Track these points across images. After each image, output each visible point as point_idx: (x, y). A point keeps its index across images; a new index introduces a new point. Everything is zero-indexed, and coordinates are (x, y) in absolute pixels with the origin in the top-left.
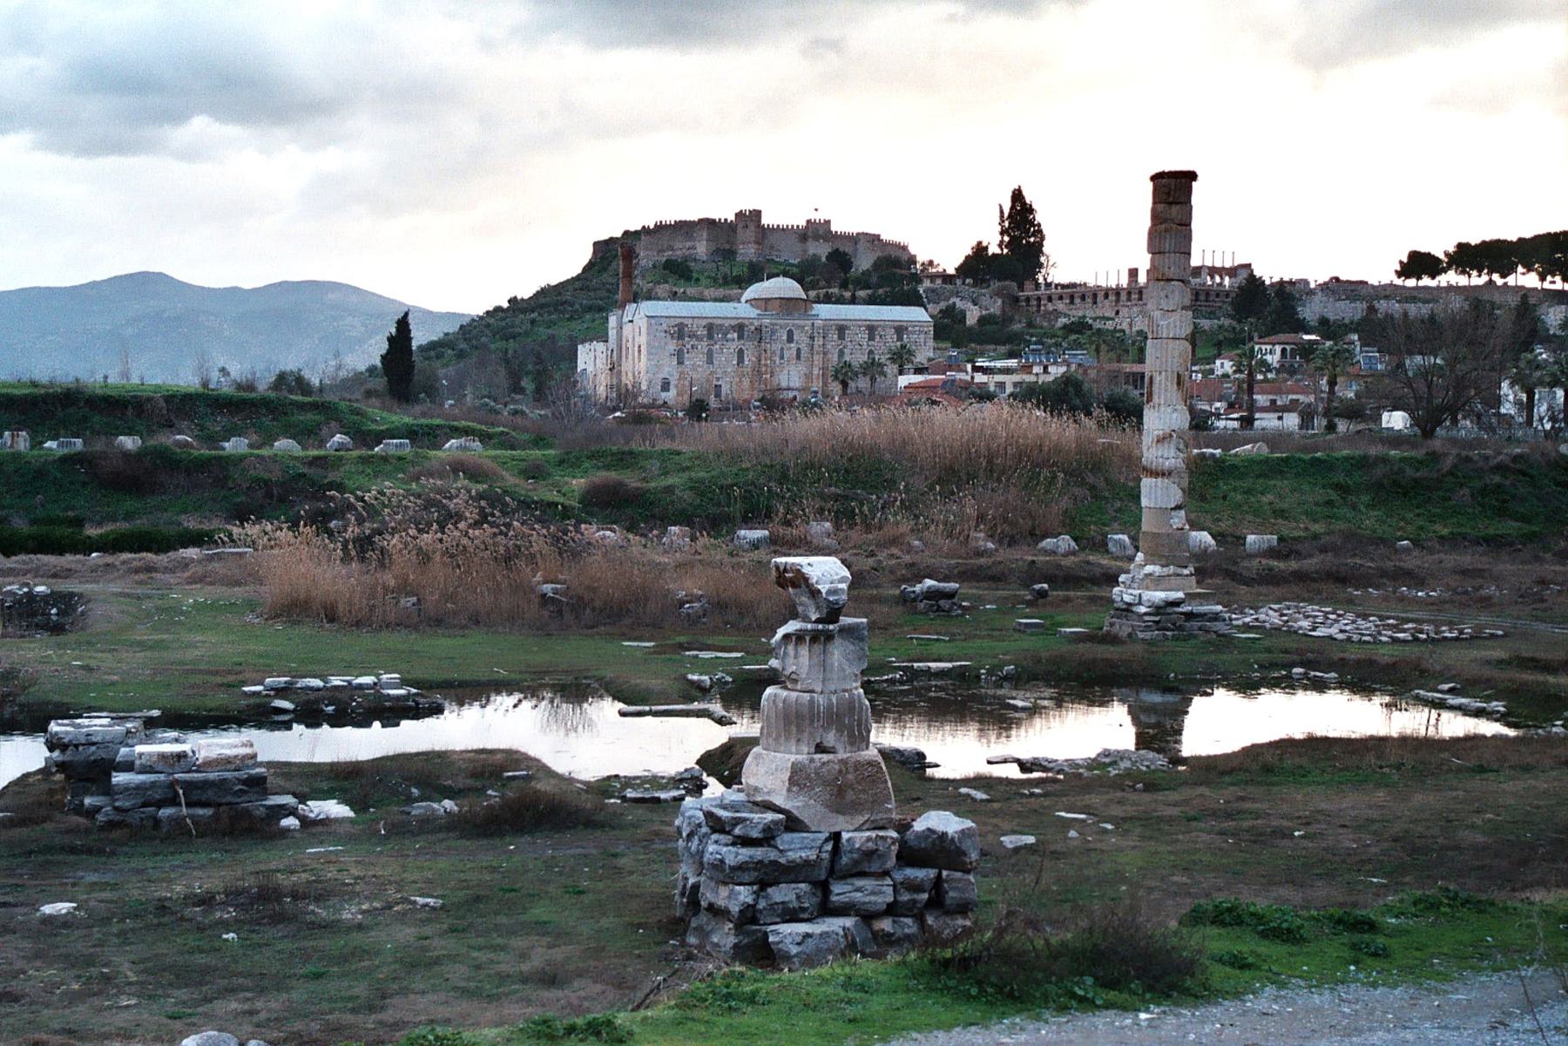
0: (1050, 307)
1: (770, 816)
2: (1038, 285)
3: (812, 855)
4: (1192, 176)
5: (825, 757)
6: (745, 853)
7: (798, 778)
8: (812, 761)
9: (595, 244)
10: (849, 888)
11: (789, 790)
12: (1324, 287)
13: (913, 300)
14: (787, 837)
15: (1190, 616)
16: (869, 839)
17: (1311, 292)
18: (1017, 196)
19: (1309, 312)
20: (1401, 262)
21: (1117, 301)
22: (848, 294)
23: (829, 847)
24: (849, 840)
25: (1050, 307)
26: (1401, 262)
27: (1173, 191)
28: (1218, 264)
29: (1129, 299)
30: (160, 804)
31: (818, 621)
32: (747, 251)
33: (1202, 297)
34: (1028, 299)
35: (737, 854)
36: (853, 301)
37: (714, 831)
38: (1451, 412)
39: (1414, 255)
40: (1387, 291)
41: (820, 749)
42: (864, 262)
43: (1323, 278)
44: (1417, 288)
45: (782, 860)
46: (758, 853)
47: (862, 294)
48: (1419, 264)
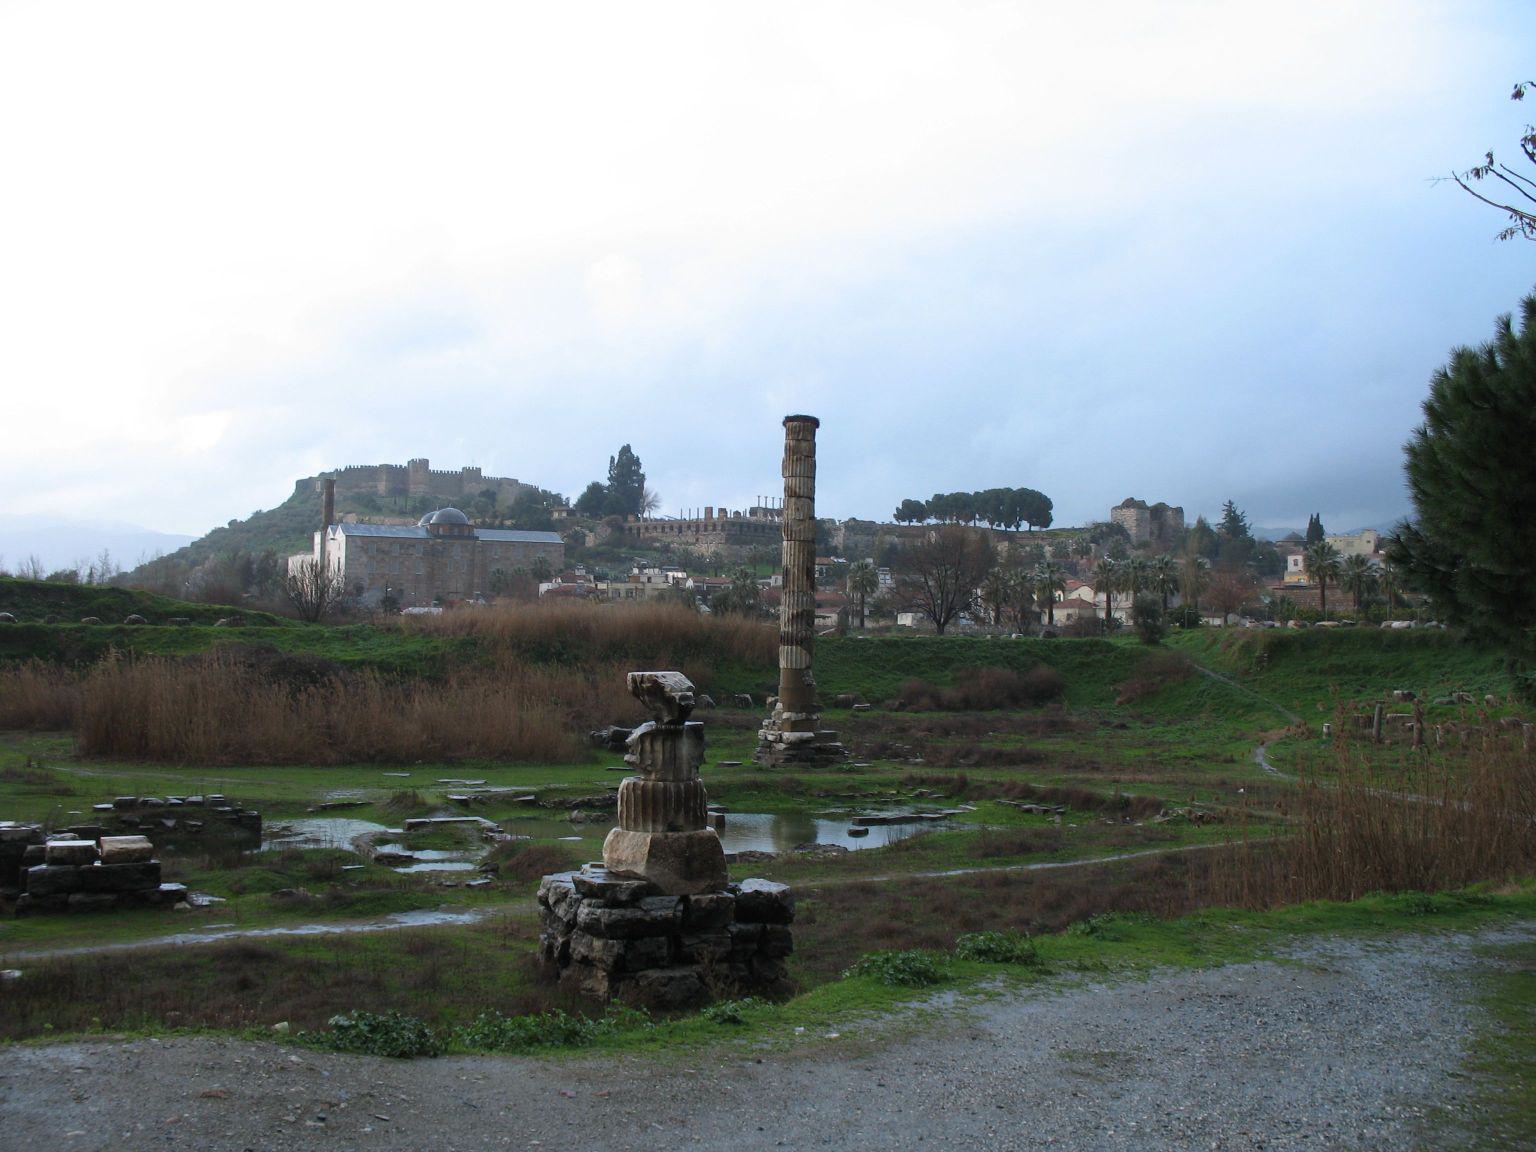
0: (647, 535)
1: (636, 883)
2: (638, 519)
3: (669, 913)
4: (626, 450)
5: (676, 835)
6: (617, 913)
7: (656, 851)
8: (666, 837)
9: (298, 482)
10: (697, 941)
11: (648, 861)
12: (846, 524)
13: (548, 526)
14: (649, 900)
15: (819, 750)
16: (711, 900)
17: (838, 529)
18: (626, 450)
19: (838, 540)
20: (897, 509)
21: (697, 531)
22: (497, 522)
23: (681, 907)
24: (697, 900)
25: (647, 535)
26: (897, 509)
27: (802, 430)
28: (770, 506)
29: (706, 530)
30: (70, 891)
31: (669, 723)
32: (417, 490)
33: (752, 529)
34: (630, 529)
35: (610, 914)
36: (502, 527)
37: (585, 896)
38: (951, 614)
39: (907, 504)
40: (888, 529)
41: (672, 828)
42: (507, 500)
43: (845, 519)
44: (909, 527)
45: (648, 918)
46: (629, 913)
47: (508, 523)
48: (910, 509)
